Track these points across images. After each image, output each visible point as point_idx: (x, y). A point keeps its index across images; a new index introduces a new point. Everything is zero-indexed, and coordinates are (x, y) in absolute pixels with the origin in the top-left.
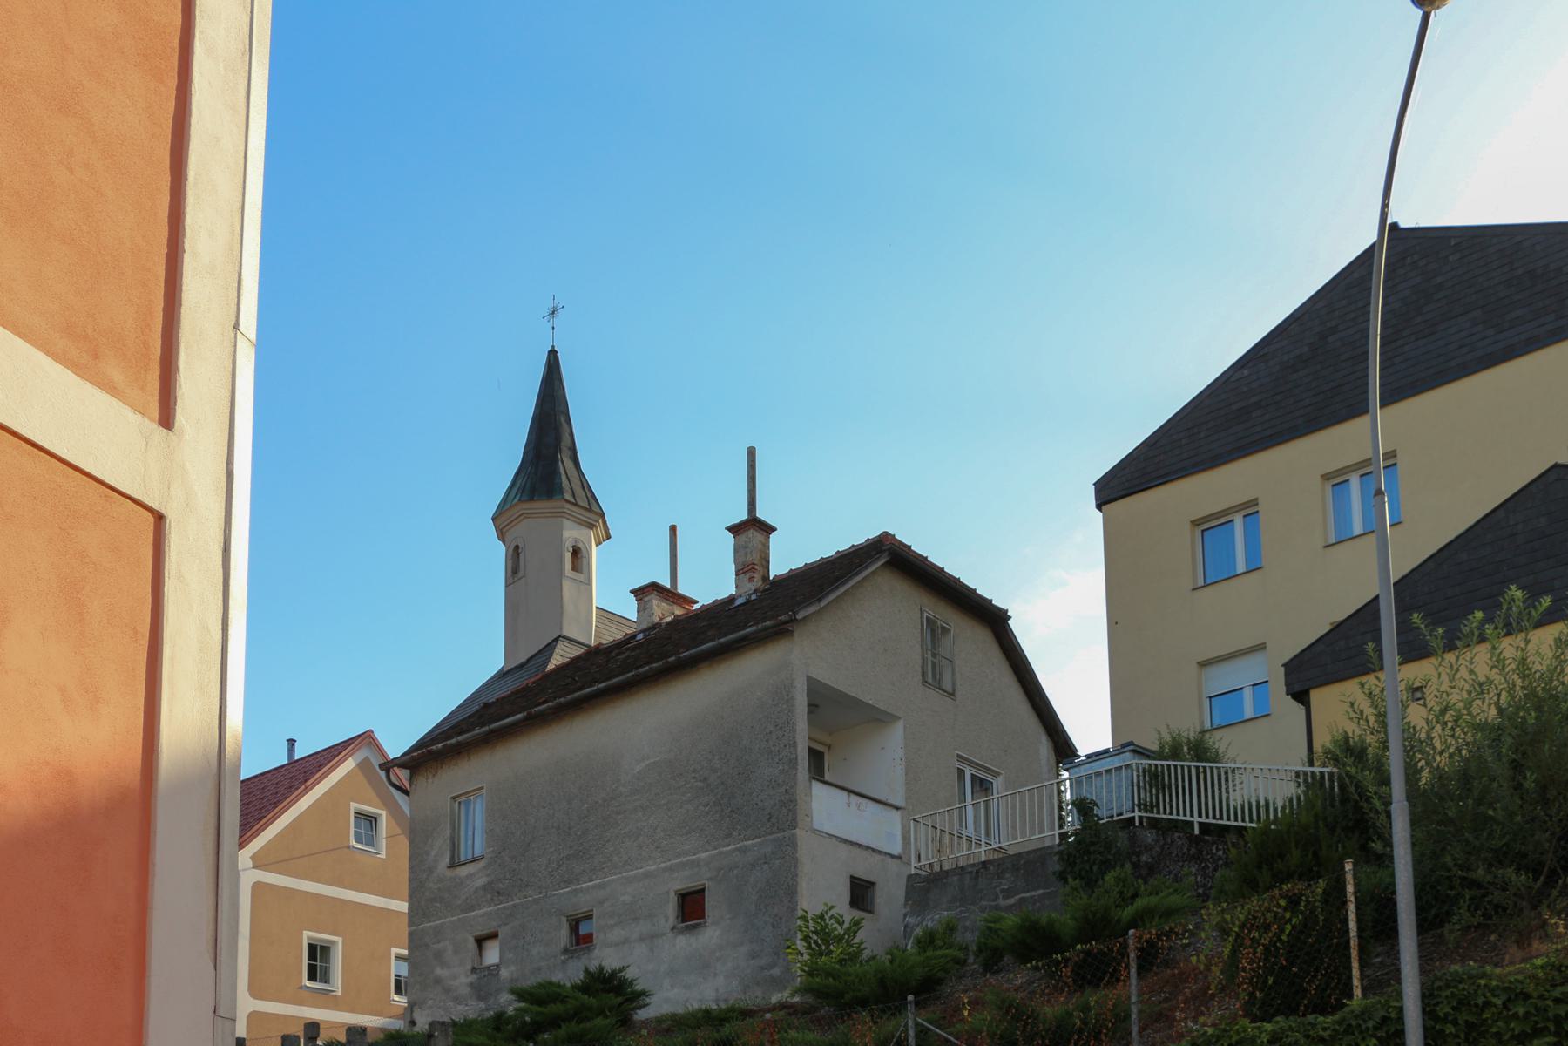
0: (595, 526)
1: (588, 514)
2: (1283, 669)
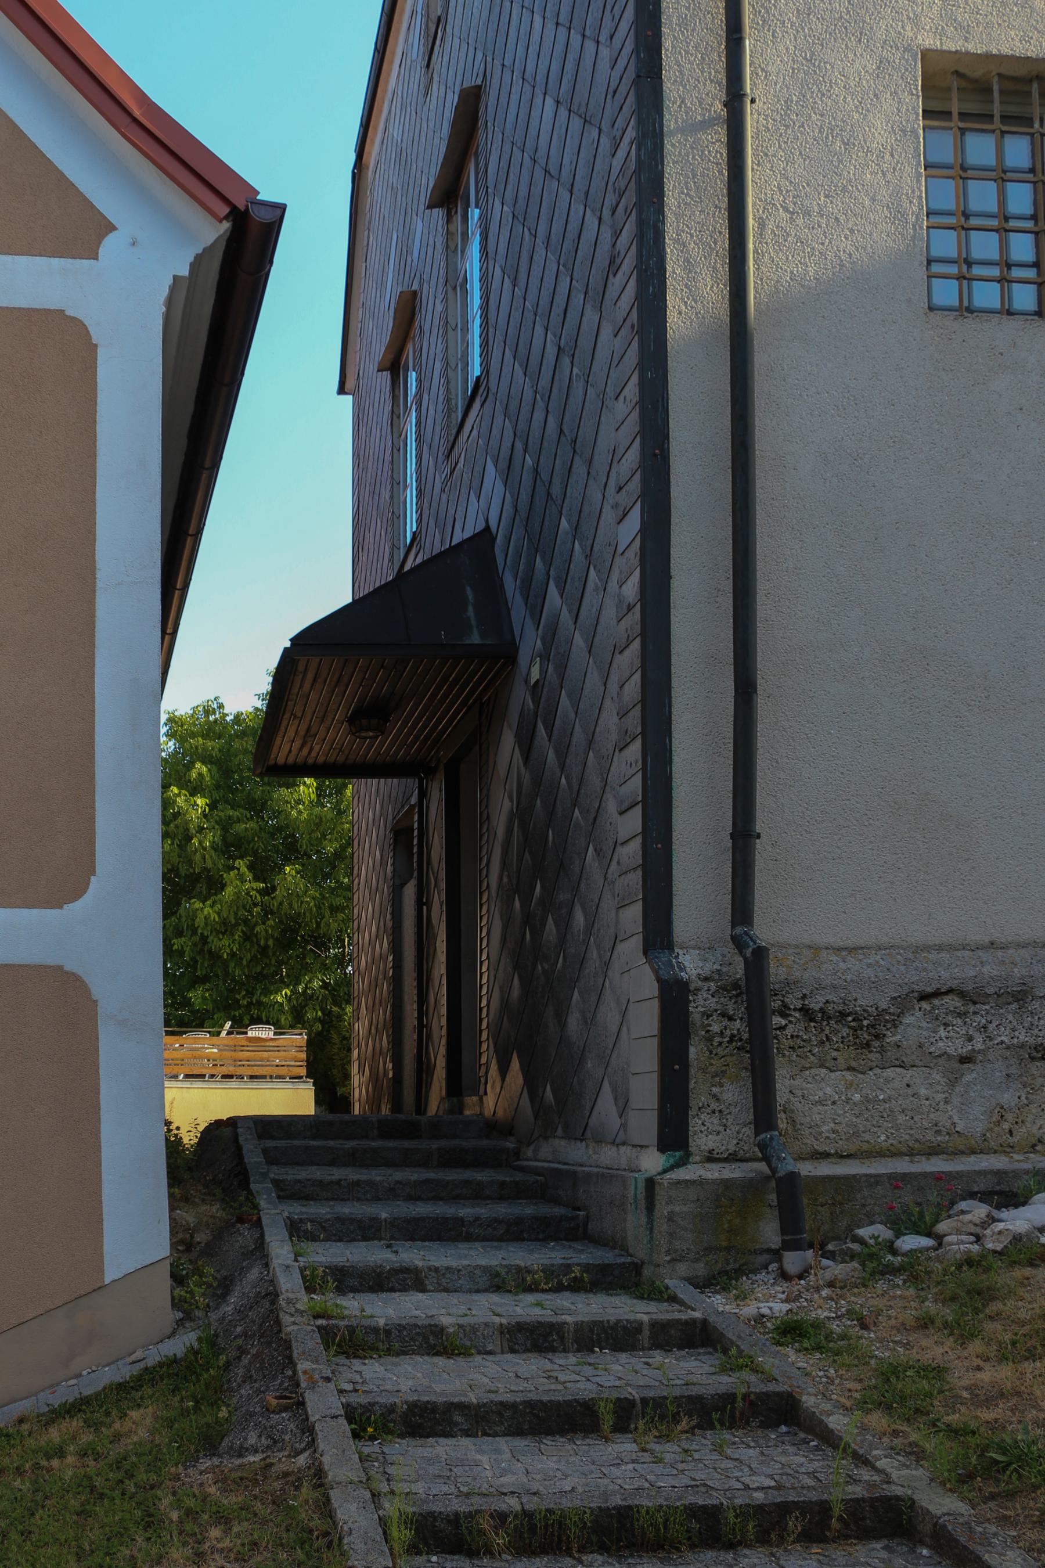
2: (102, 251)
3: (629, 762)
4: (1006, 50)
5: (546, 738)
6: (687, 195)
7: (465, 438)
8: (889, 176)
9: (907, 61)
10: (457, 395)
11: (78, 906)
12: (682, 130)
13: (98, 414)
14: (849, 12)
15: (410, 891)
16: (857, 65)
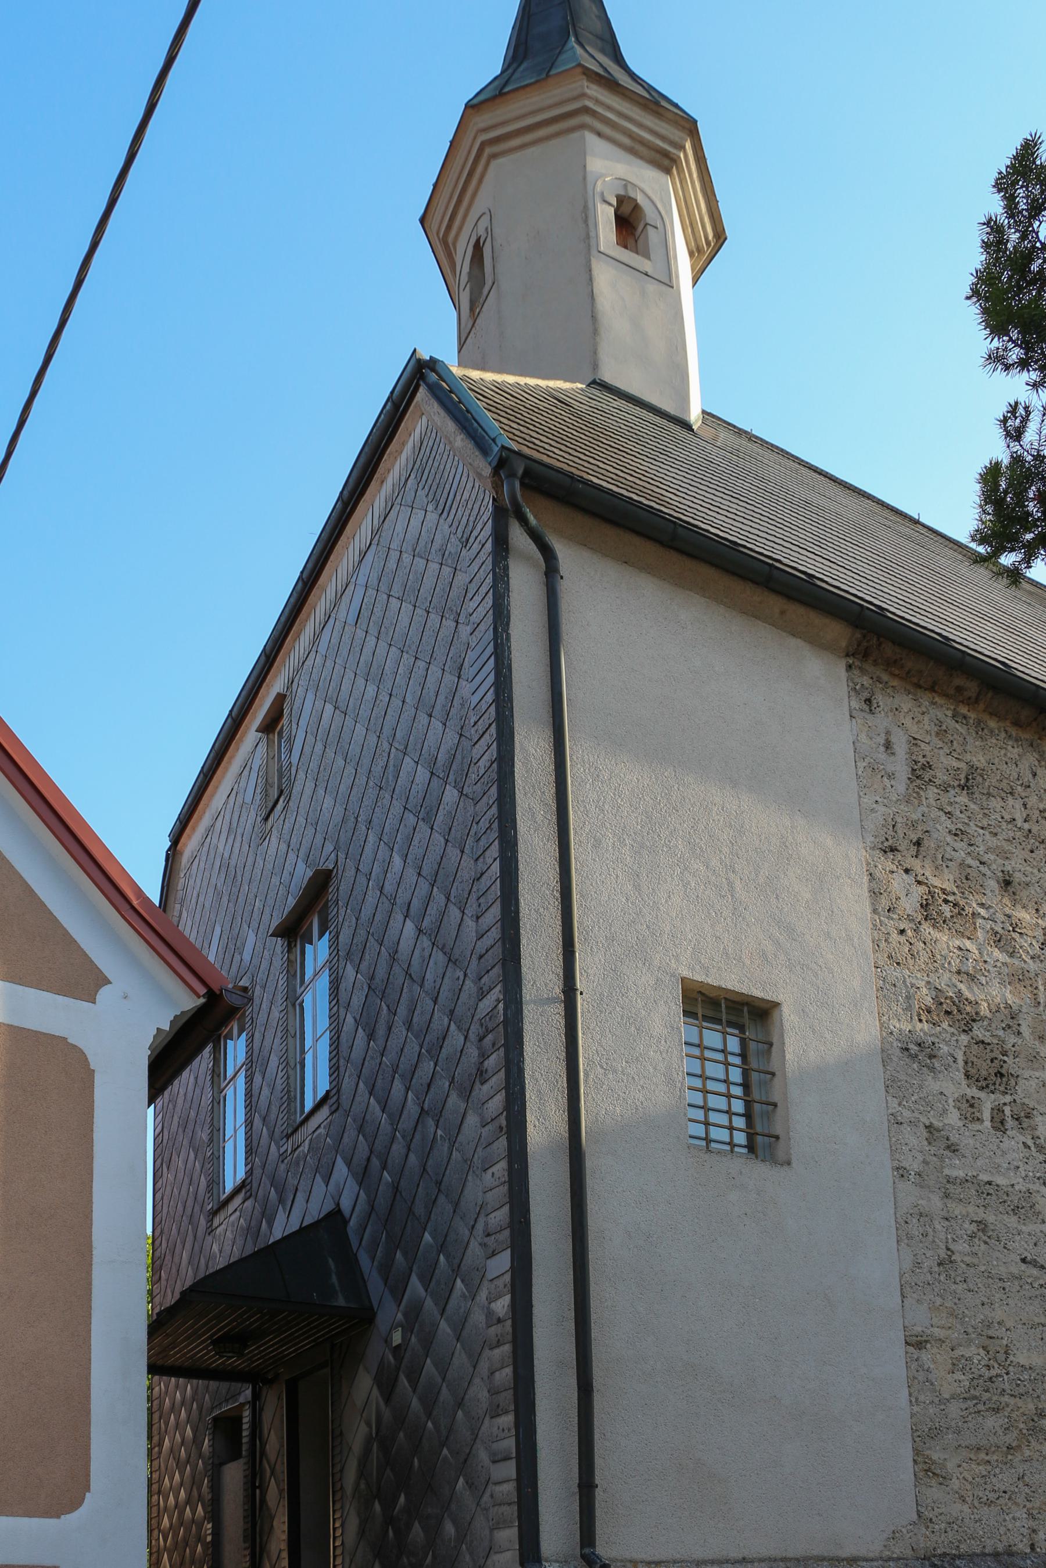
0: (674, 161)
1: (649, 120)
2: (99, 997)
3: (501, 1428)
4: (730, 987)
5: (410, 1389)
6: (538, 1046)
7: (311, 1130)
8: (664, 1055)
9: (673, 982)
10: (295, 1089)
11: (81, 1509)
12: (535, 1002)
13: (95, 1125)
14: (637, 945)
15: (234, 1474)
16: (643, 979)
